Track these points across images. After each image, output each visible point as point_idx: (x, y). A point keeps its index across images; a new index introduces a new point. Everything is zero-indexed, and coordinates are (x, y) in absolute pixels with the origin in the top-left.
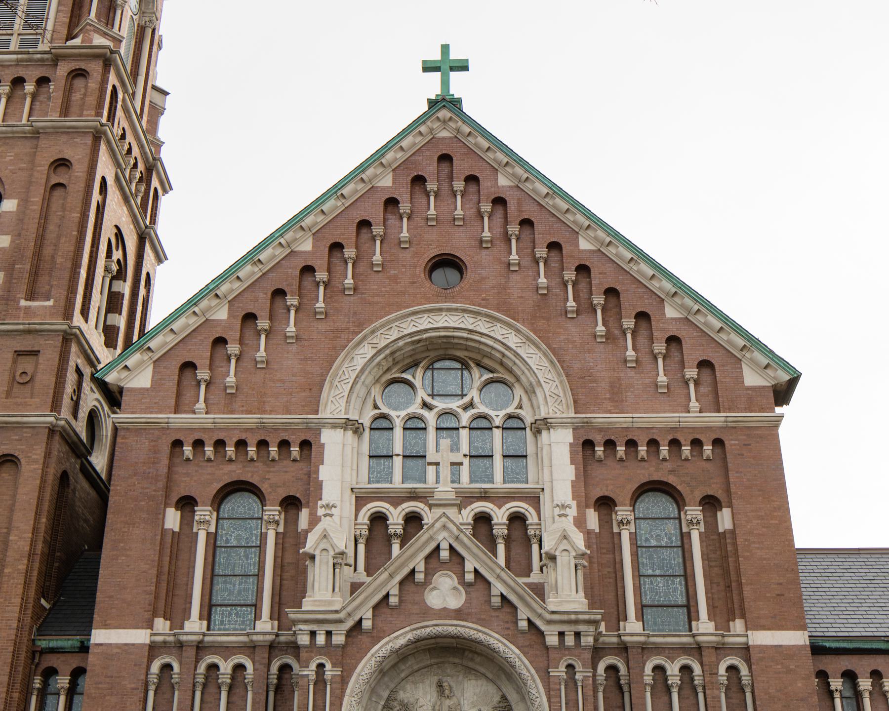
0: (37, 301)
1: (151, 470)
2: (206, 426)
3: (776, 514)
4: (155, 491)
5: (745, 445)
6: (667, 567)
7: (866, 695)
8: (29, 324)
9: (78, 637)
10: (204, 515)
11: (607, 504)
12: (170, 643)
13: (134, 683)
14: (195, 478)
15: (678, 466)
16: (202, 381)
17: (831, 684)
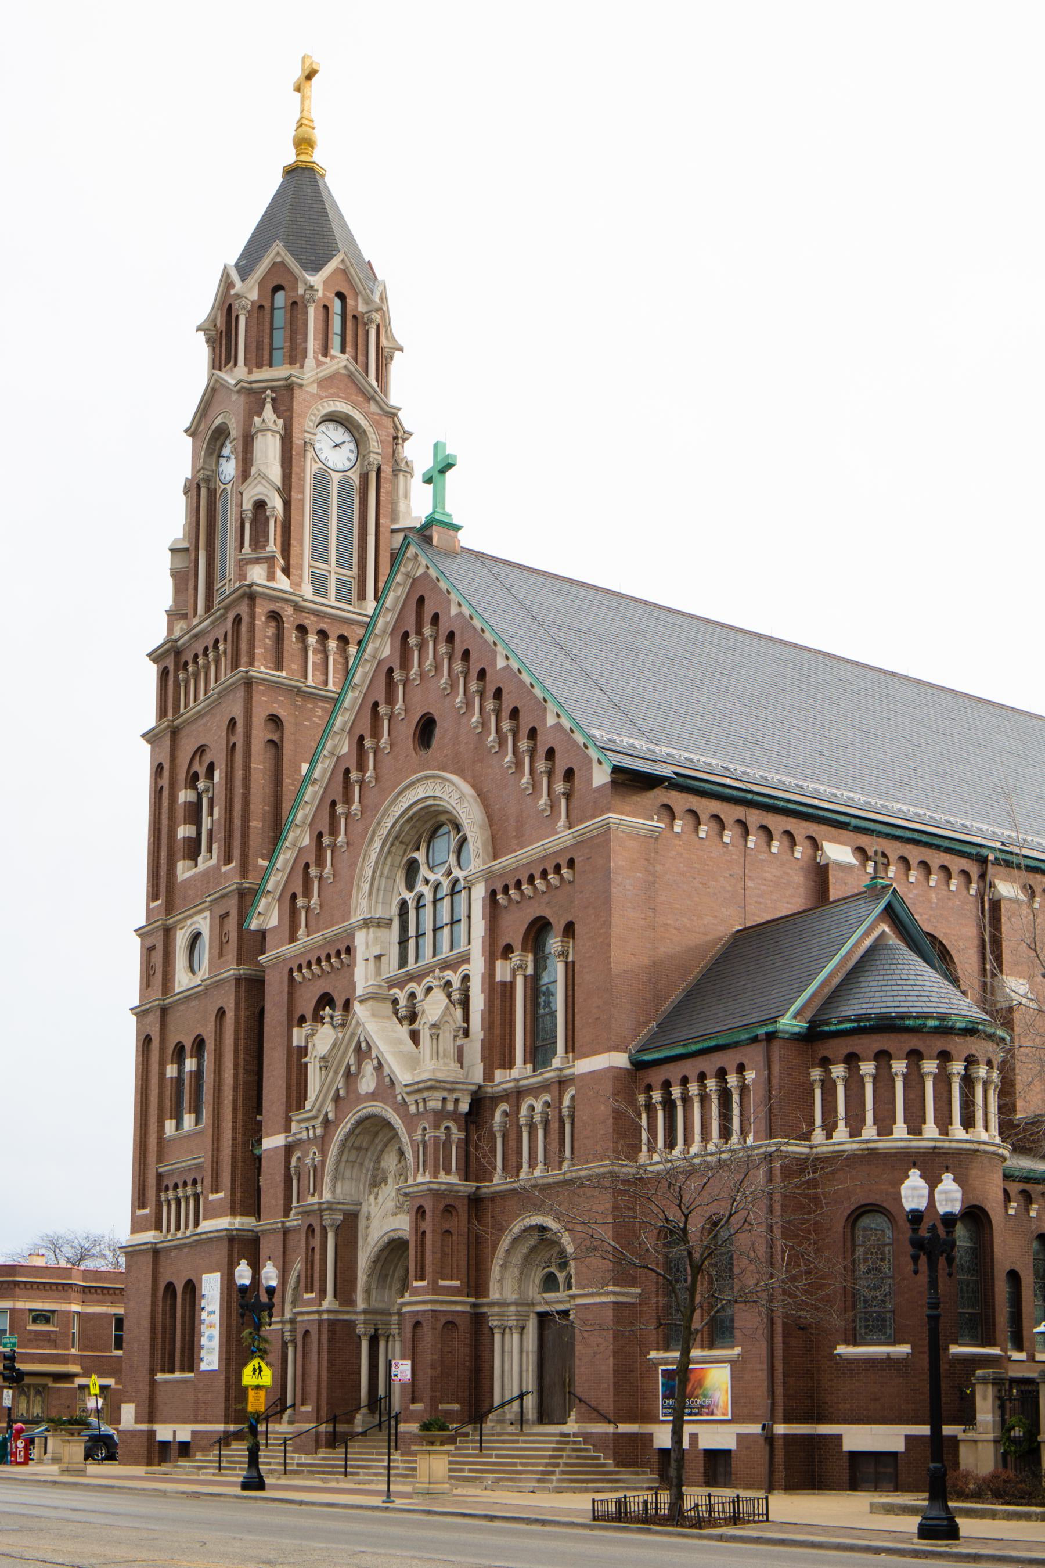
2: (297, 952)
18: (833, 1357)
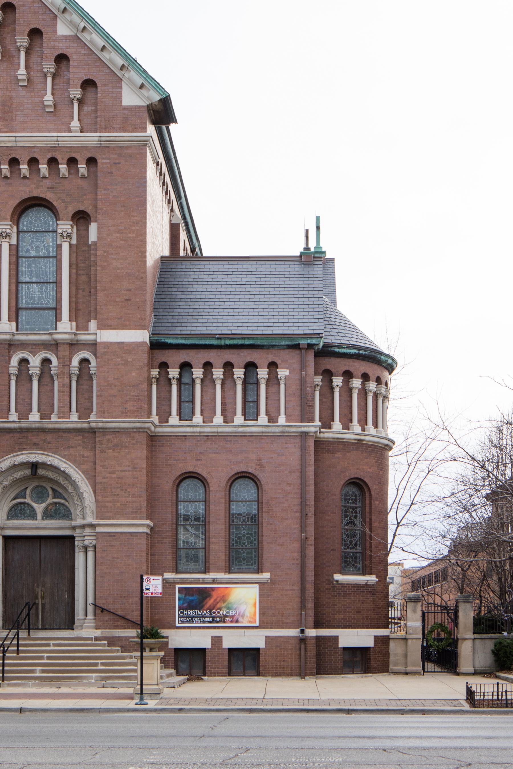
3: (134, 228)
5: (115, 163)
6: (42, 275)
7: (198, 382)
10: (6, 229)
11: (86, 218)
15: (56, 183)
17: (170, 373)
18: (331, 581)
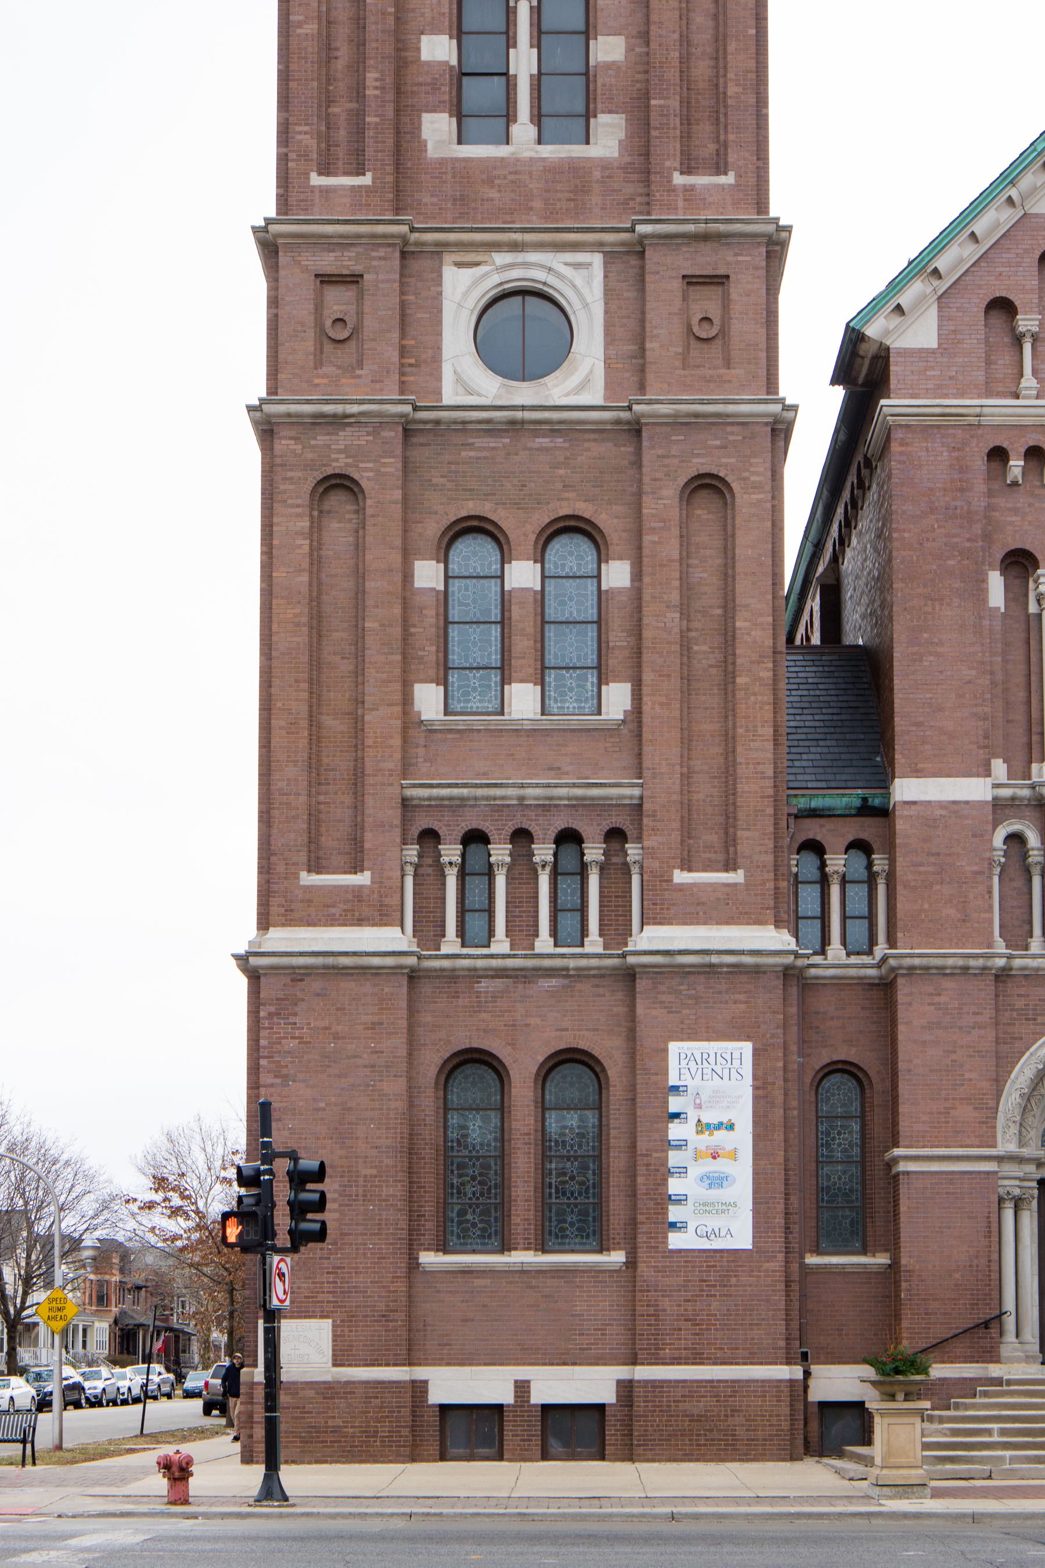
0: (697, 174)
1: (958, 503)
4: (969, 540)
8: (706, 221)
9: (859, 791)
11: (1025, 566)
12: (1021, 799)
13: (977, 864)
14: (1030, 518)
16: (1028, 335)
